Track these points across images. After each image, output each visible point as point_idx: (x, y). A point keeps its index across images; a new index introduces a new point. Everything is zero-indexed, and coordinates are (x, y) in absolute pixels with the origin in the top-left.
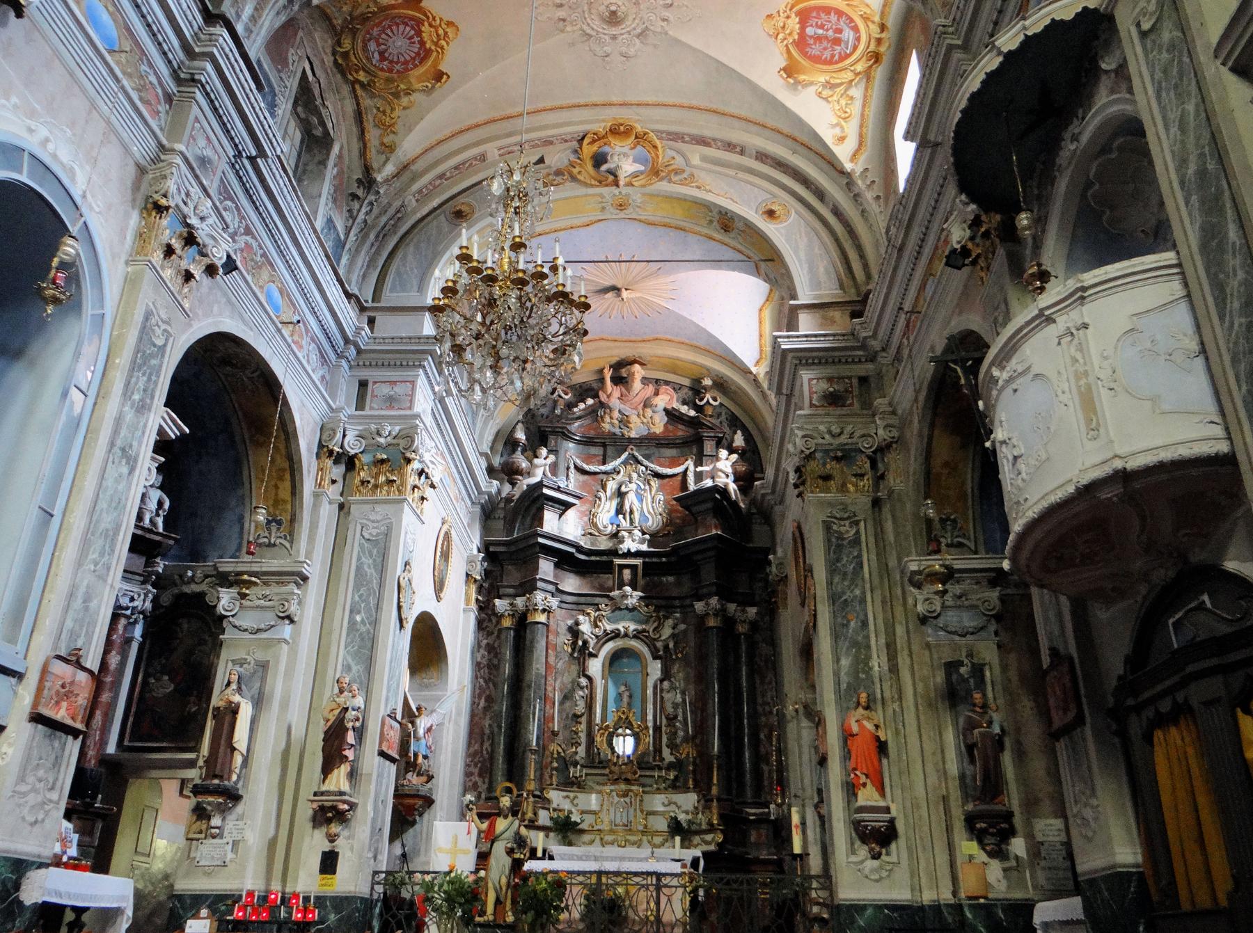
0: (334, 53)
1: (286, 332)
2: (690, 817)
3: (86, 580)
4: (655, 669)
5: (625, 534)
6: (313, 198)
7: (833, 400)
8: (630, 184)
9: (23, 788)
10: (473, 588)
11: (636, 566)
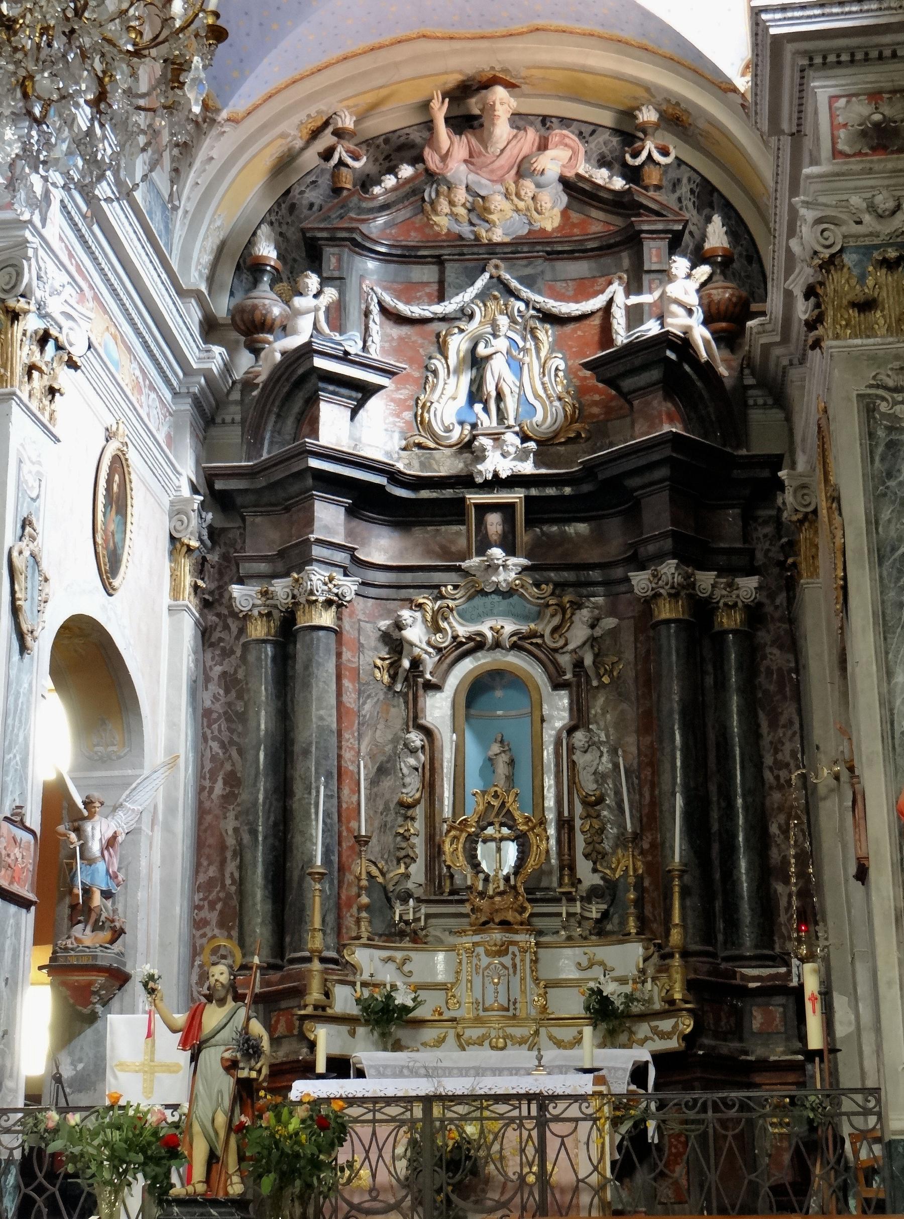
2: (628, 989)
4: (558, 709)
5: (486, 442)
7: (881, 137)
10: (186, 565)
11: (512, 506)
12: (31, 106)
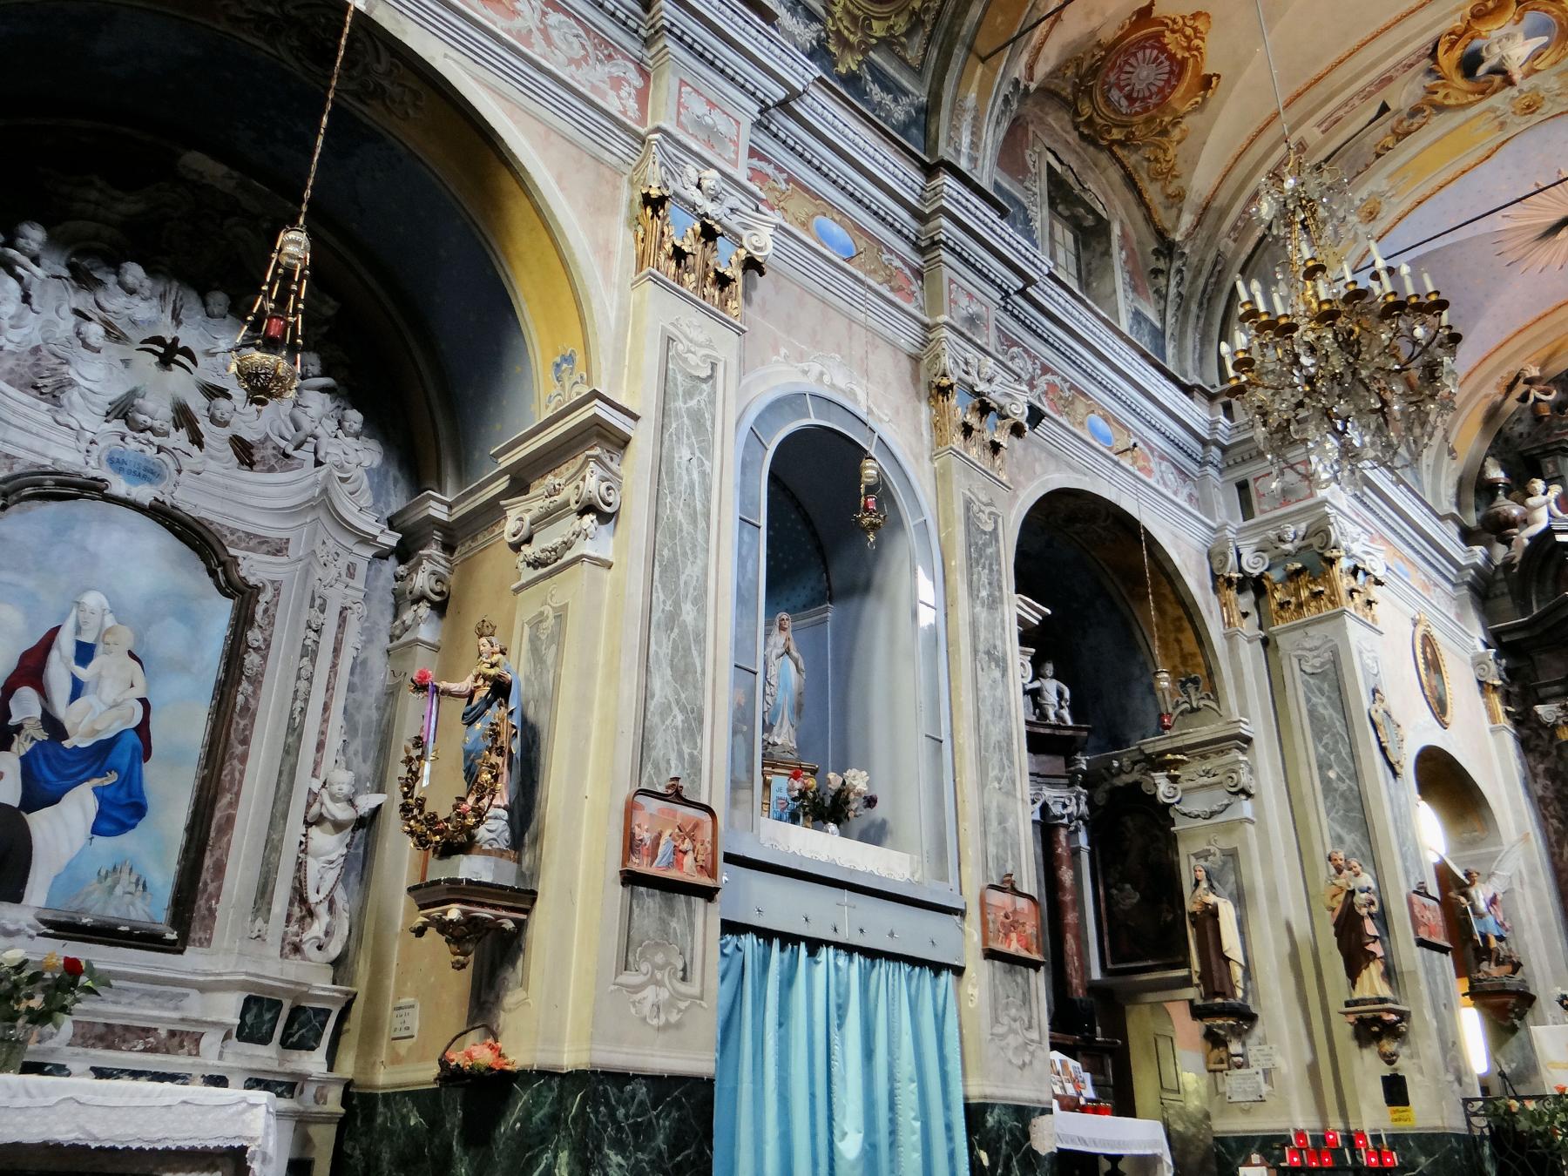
0: (1076, 128)
1: (1125, 462)
3: (995, 800)
6: (1108, 300)
8: (1533, 71)
9: (1000, 1030)
10: (1496, 699)
12: (1565, 381)
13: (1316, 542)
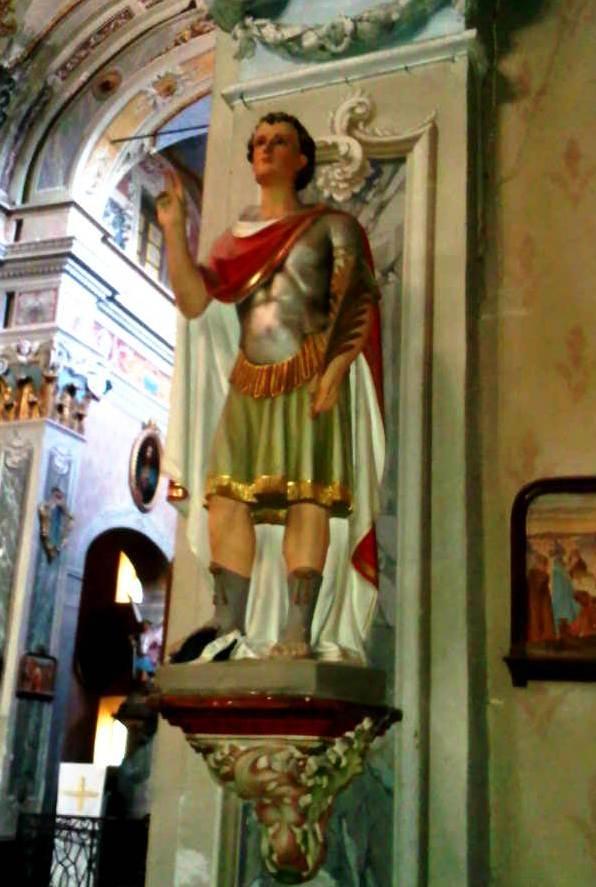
13: (41, 359)
